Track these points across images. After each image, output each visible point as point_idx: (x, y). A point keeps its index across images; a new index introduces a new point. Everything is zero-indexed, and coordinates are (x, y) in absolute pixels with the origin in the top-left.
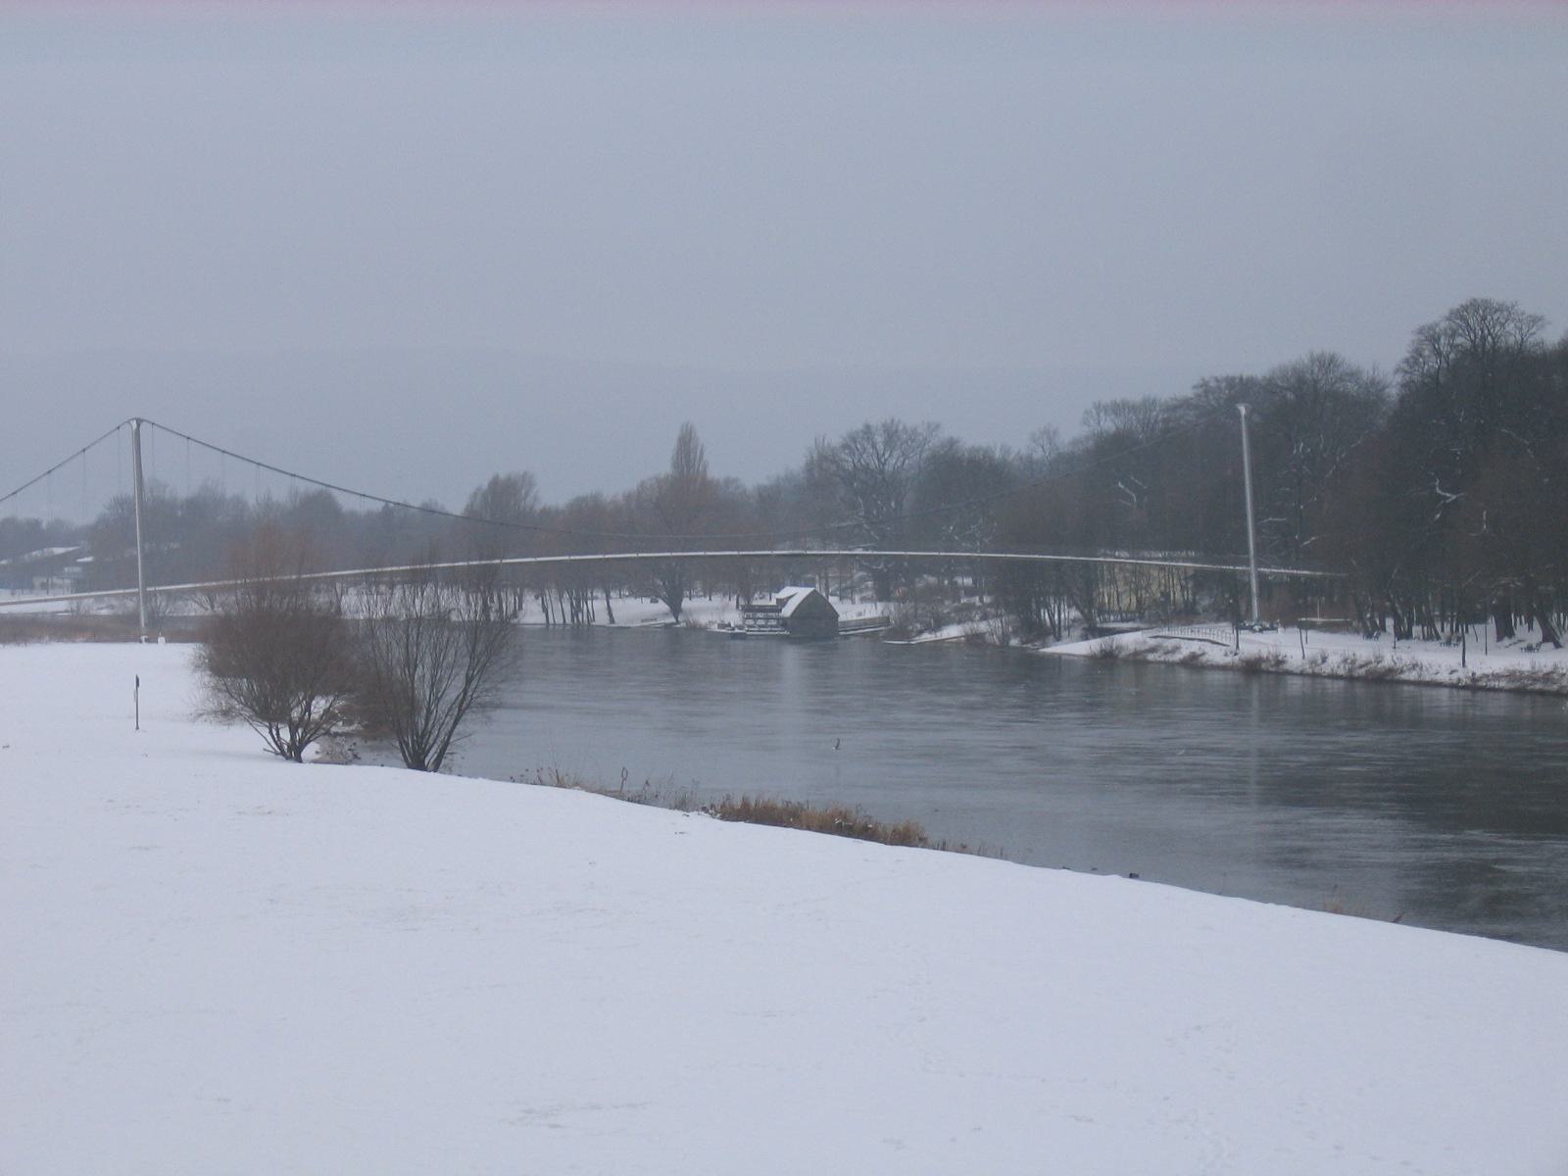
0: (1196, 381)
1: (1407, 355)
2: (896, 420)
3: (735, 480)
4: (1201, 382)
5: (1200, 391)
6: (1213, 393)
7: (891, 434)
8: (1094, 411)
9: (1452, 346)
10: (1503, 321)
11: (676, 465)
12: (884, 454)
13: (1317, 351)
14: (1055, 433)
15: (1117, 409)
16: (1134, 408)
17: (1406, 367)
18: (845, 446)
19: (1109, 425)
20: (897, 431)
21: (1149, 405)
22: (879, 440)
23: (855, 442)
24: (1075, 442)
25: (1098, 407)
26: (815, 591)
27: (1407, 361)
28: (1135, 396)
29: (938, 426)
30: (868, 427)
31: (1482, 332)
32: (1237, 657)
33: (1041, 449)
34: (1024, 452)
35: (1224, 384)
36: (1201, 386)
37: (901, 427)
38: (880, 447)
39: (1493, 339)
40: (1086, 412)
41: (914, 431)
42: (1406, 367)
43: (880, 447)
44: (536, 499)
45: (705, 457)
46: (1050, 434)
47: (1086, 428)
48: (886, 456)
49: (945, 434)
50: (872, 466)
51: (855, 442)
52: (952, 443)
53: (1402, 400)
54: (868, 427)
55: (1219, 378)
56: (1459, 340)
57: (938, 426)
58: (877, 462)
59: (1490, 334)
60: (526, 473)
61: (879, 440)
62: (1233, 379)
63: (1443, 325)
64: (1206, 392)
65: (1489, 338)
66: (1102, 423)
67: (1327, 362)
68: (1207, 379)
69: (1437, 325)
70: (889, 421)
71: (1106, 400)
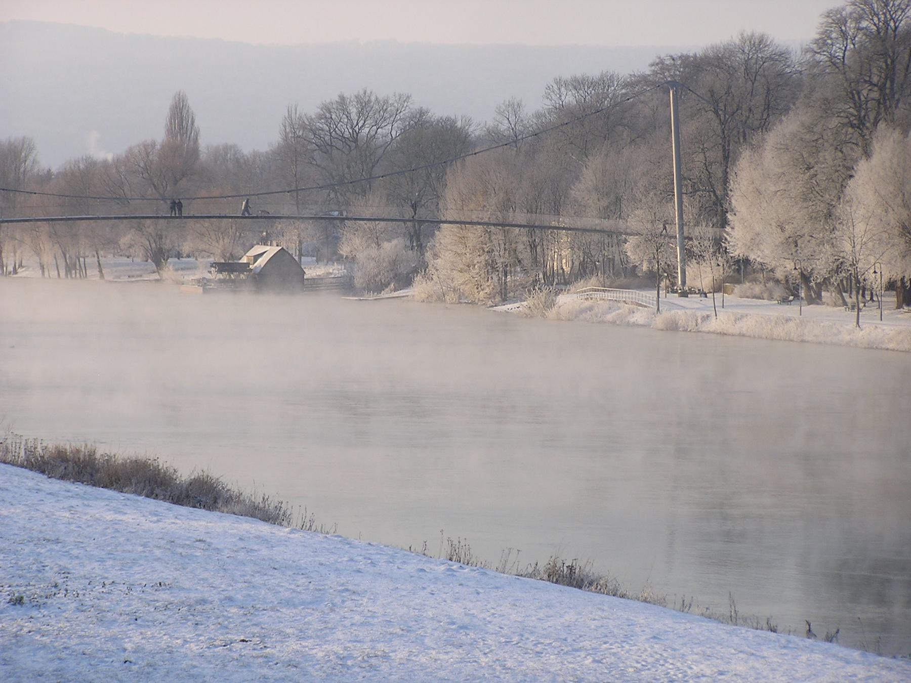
0: (653, 59)
1: (817, 36)
2: (368, 92)
3: (233, 147)
4: (658, 61)
5: (656, 68)
6: (669, 70)
7: (364, 105)
8: (555, 87)
9: (859, 29)
10: (904, 7)
11: (170, 131)
12: (357, 124)
13: (748, 33)
14: (519, 105)
15: (578, 84)
16: (593, 84)
17: (814, 47)
18: (320, 117)
19: (570, 98)
20: (369, 101)
21: (605, 81)
22: (353, 111)
23: (330, 112)
24: (538, 116)
25: (559, 82)
26: (282, 248)
27: (816, 42)
28: (595, 73)
29: (408, 97)
30: (342, 98)
31: (886, 16)
32: (153, 659)
33: (507, 122)
34: (491, 124)
35: (679, 62)
36: (657, 64)
37: (373, 99)
38: (354, 116)
39: (895, 23)
40: (548, 88)
41: (386, 102)
42: (814, 47)
43: (354, 116)
44: (34, 162)
45: (196, 124)
46: (515, 107)
47: (548, 102)
48: (360, 125)
49: (416, 104)
50: (347, 135)
51: (330, 112)
52: (422, 113)
53: (163, 147)
54: (342, 98)
55: (675, 56)
56: (864, 24)
57: (408, 97)
58: (351, 131)
59: (892, 18)
60: (24, 138)
61: (353, 111)
62: (688, 57)
63: (849, 9)
64: (661, 69)
65: (892, 24)
66: (563, 98)
67: (757, 42)
68: (662, 56)
69: (844, 9)
70: (362, 92)
71: (567, 76)
